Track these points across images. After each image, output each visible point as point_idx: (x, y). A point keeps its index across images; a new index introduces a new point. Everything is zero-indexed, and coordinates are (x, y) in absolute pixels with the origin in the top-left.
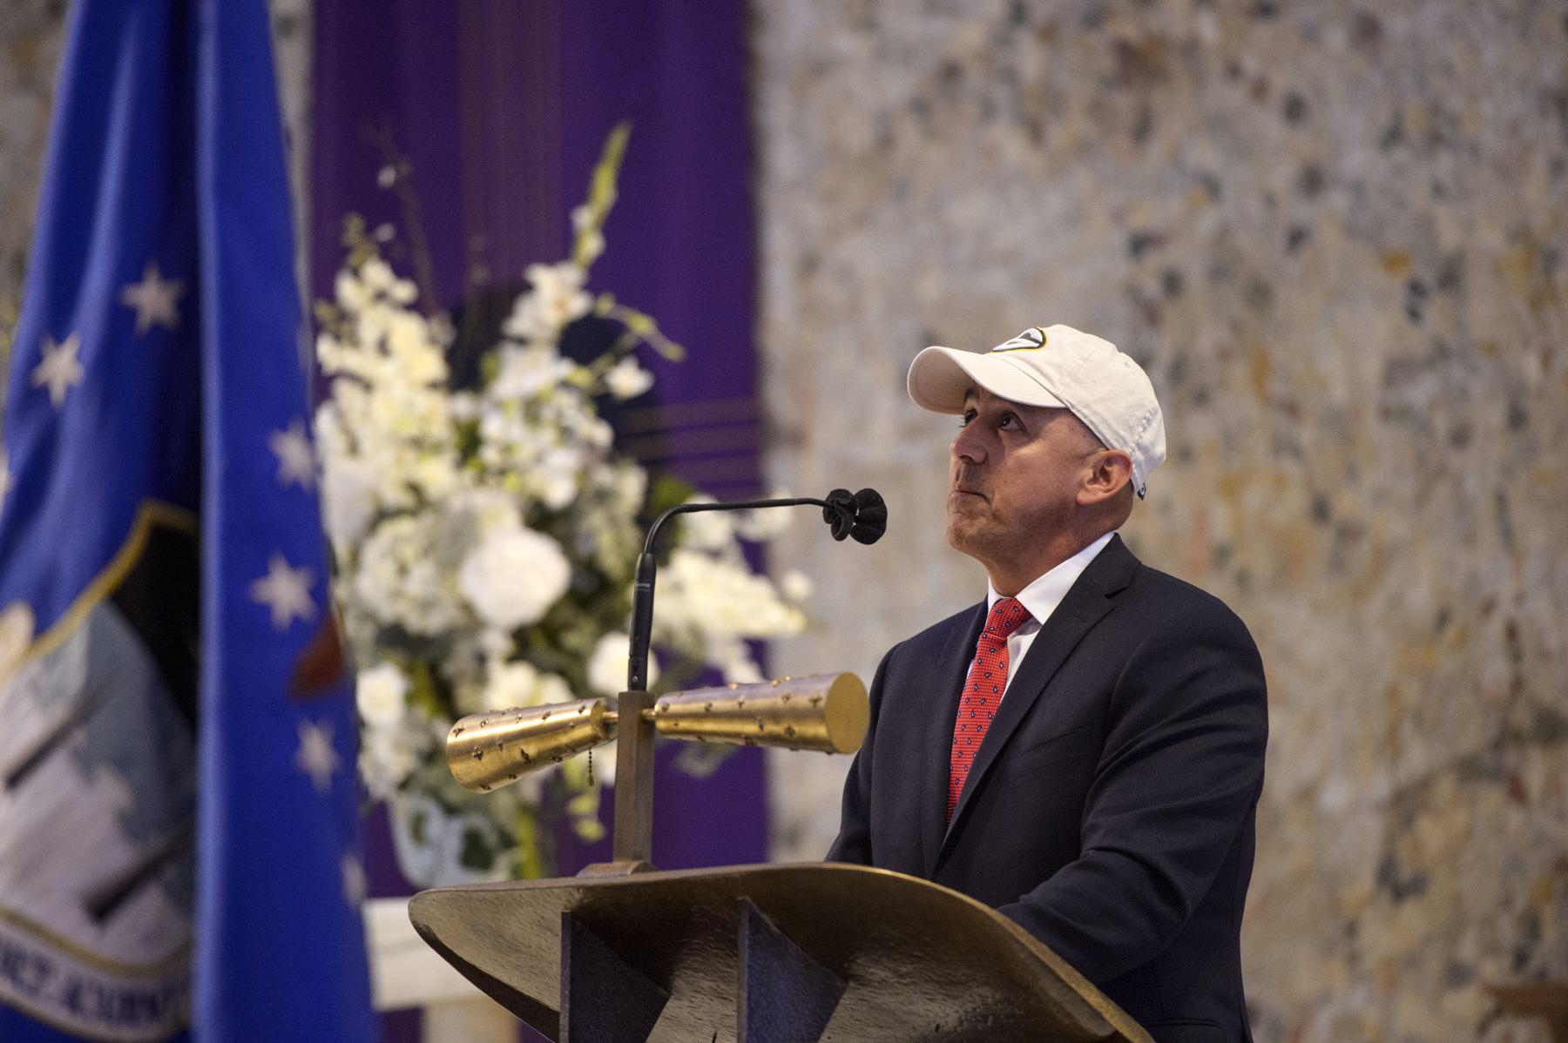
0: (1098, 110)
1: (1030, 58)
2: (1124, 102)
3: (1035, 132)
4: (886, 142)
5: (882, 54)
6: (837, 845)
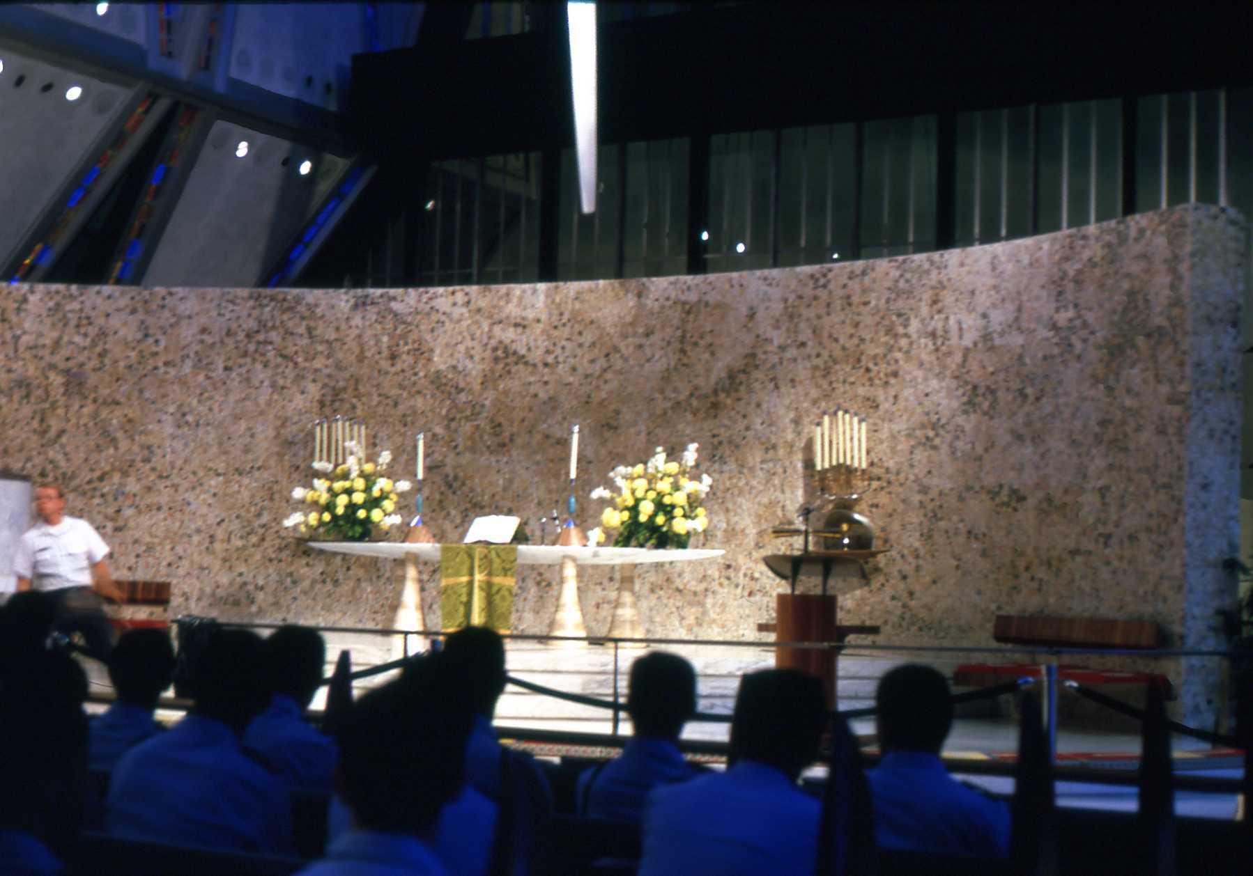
0: (706, 412)
1: (695, 403)
2: (712, 411)
3: (695, 415)
4: (665, 413)
5: (665, 398)
6: (1077, 762)
